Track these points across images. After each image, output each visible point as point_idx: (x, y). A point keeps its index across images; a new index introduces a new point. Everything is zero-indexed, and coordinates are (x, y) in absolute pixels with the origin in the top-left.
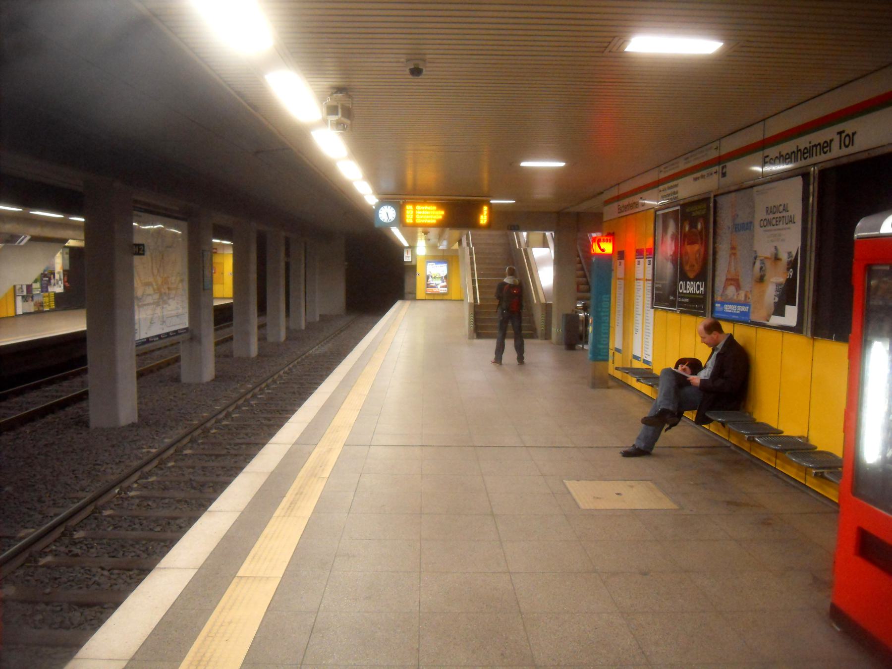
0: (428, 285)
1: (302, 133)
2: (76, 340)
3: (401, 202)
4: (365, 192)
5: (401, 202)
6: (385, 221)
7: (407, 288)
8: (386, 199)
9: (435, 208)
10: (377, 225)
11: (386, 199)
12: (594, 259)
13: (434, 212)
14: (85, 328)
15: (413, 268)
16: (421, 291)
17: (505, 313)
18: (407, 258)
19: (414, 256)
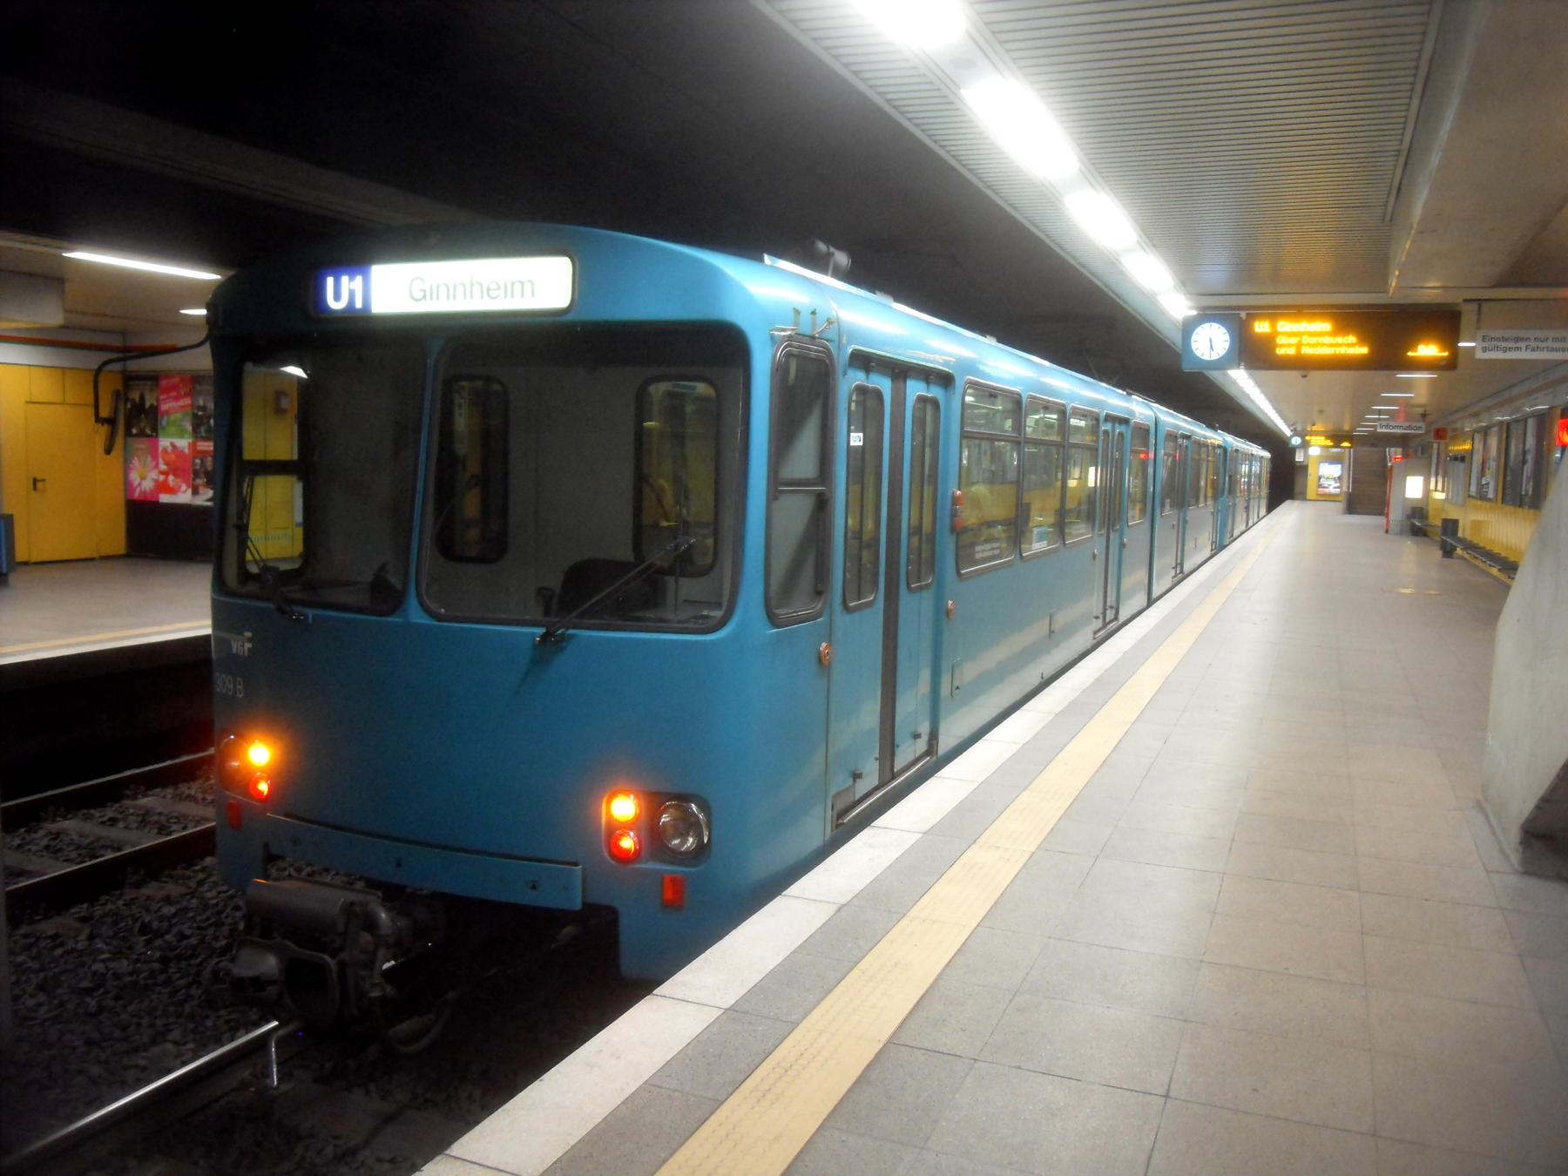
0: (1320, 486)
1: (1048, 197)
2: (177, 666)
3: (1243, 314)
4: (1287, 432)
5: (1243, 314)
6: (1206, 357)
7: (1297, 489)
8: (1296, 433)
9: (1326, 326)
10: (1187, 367)
11: (1296, 433)
12: (1245, 469)
13: (1328, 340)
14: (209, 631)
15: (1304, 468)
16: (1311, 493)
17: (1367, 494)
18: (1299, 457)
19: (1306, 455)
